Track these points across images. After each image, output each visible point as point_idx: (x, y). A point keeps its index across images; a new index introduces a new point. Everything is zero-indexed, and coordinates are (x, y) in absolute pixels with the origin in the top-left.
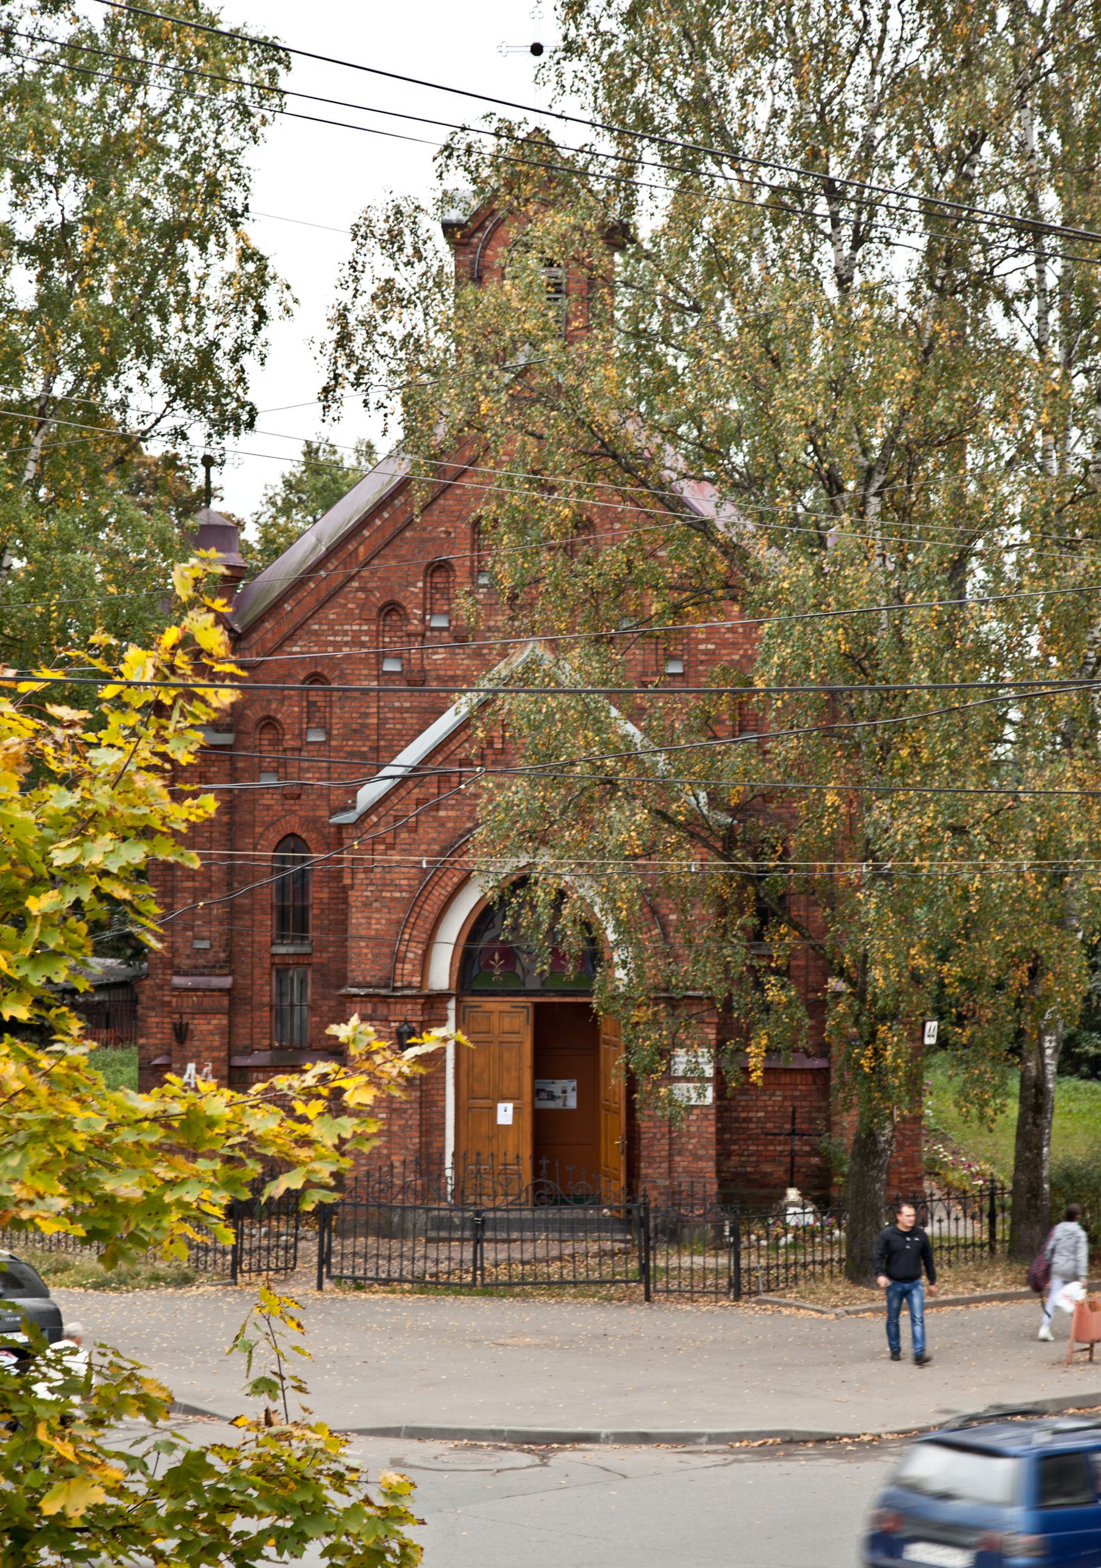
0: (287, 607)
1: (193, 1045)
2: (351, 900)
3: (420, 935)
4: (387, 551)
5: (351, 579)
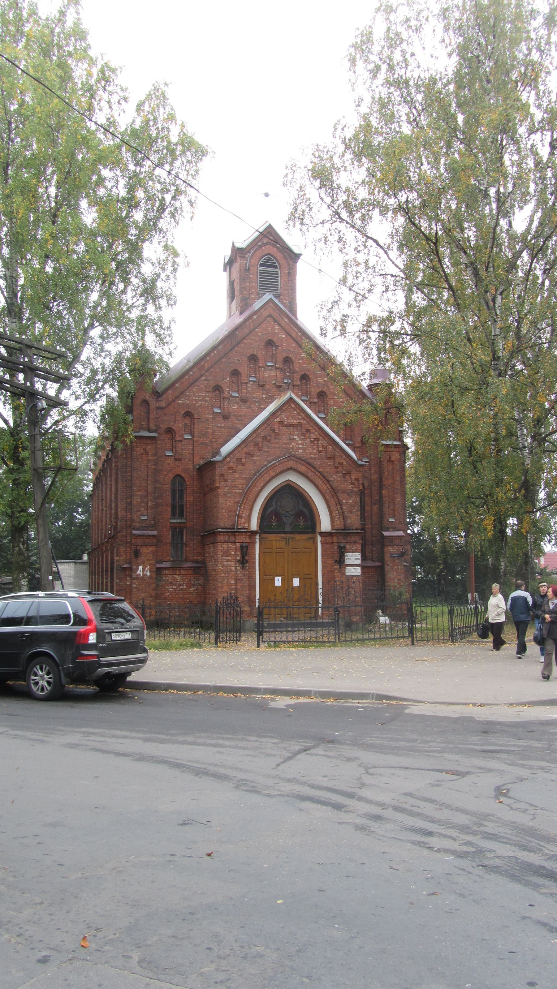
0: (177, 385)
1: (141, 559)
5: (202, 376)
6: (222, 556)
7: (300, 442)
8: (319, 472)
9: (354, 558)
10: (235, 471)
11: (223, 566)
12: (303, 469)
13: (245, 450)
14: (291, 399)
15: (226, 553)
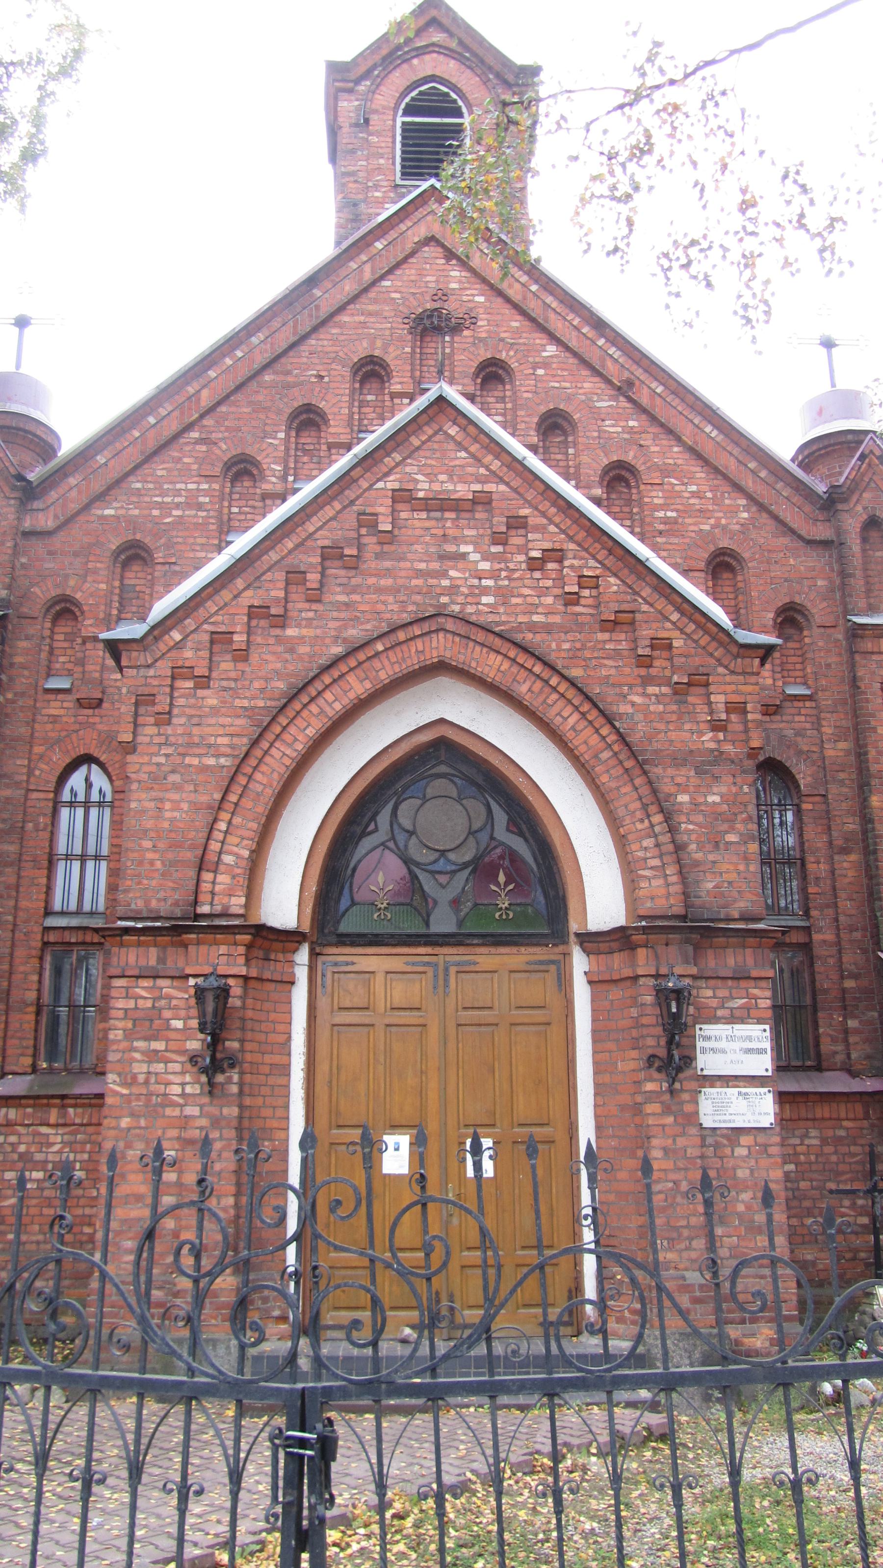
0: (101, 459)
2: (130, 769)
3: (247, 825)
4: (239, 396)
5: (189, 427)
6: (129, 1035)
7: (485, 566)
8: (572, 683)
9: (737, 1048)
10: (203, 682)
11: (130, 1081)
12: (492, 665)
13: (250, 598)
14: (441, 400)
15: (149, 1024)
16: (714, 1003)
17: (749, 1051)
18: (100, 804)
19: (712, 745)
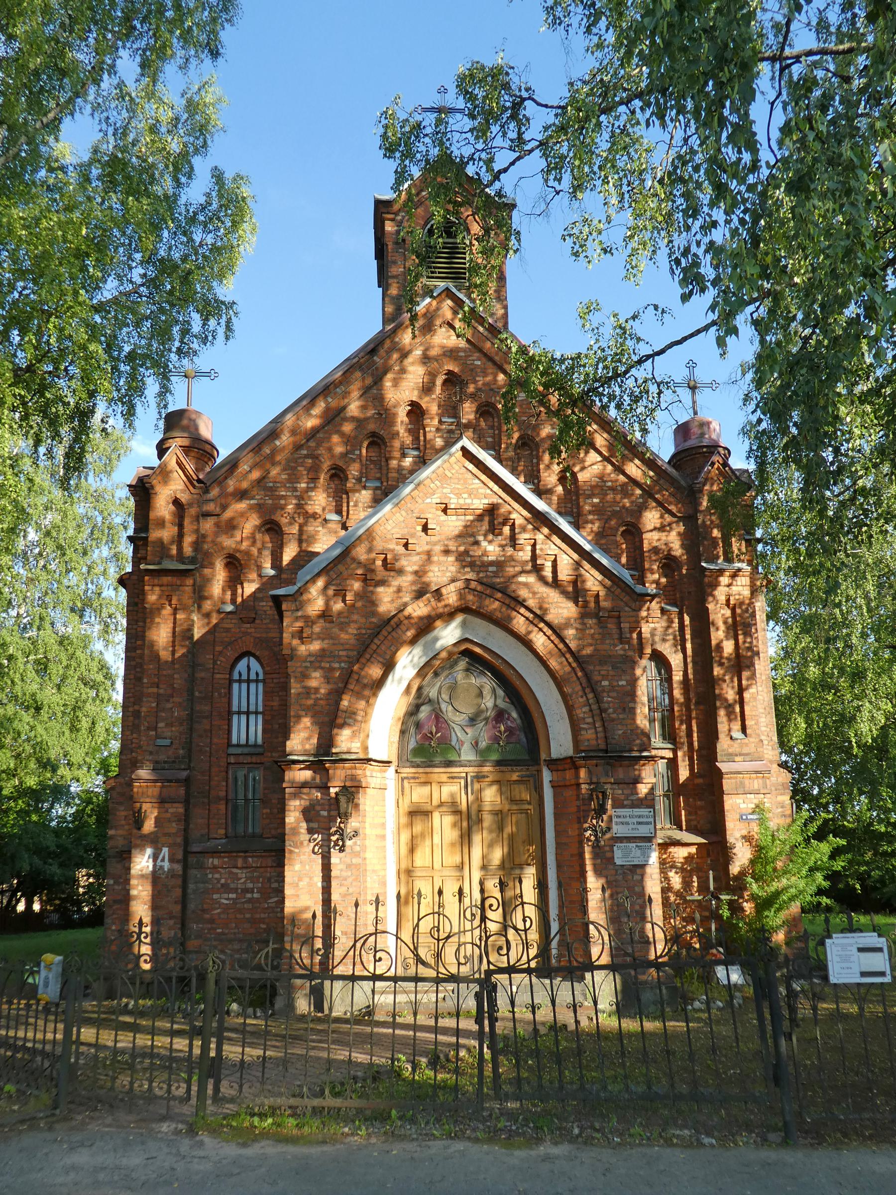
2: (290, 671)
16: (622, 797)
17: (640, 823)
18: (257, 681)
19: (622, 652)
